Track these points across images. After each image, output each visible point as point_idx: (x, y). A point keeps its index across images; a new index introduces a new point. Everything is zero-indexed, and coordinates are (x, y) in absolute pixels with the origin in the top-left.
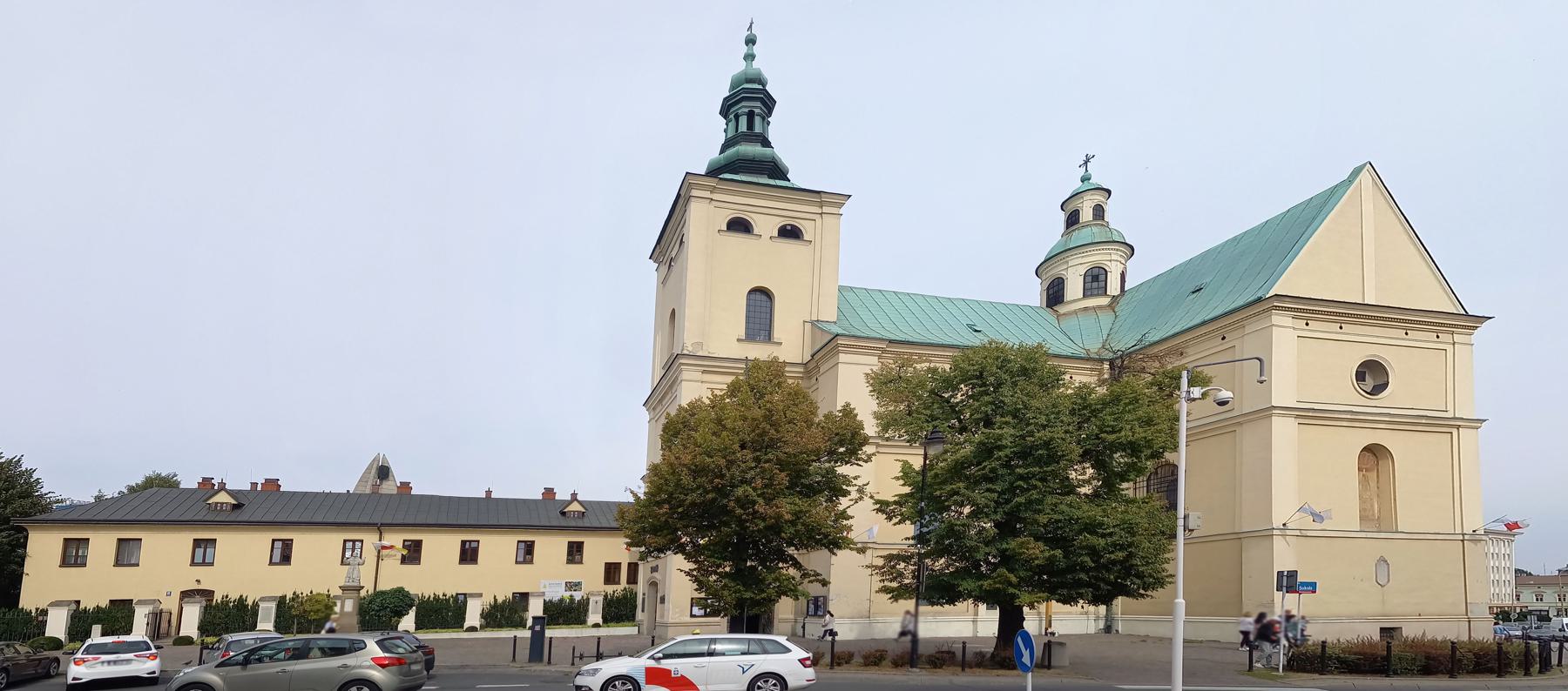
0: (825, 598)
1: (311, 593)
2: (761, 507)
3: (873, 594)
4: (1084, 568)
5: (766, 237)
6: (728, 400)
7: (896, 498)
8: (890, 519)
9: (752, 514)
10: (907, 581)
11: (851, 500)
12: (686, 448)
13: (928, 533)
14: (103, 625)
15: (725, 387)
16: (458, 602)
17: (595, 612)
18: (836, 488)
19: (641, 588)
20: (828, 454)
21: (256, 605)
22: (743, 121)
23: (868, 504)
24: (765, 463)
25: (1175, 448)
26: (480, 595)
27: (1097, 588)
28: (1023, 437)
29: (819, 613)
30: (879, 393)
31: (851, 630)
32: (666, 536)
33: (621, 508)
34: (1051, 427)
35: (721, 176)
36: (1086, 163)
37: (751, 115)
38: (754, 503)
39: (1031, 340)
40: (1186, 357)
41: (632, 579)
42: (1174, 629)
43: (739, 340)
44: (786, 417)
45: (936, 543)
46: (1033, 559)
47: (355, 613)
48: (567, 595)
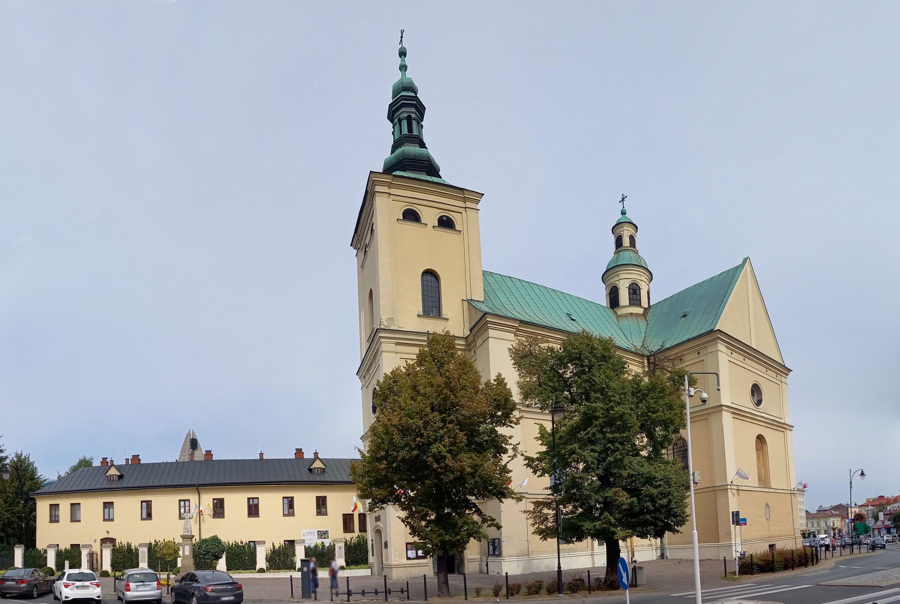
0: (499, 540)
1: (164, 541)
2: (450, 462)
3: (530, 535)
4: (649, 512)
5: (430, 226)
6: (418, 369)
7: (538, 455)
8: (535, 472)
9: (444, 468)
10: (550, 525)
11: (509, 457)
12: (394, 411)
13: (560, 484)
14: (69, 561)
15: (415, 357)
16: (250, 548)
17: (340, 557)
18: (497, 446)
19: (370, 535)
20: (491, 417)
21: (137, 550)
22: (405, 124)
23: (520, 461)
24: (449, 424)
25: (685, 426)
26: (264, 542)
27: (656, 525)
28: (608, 410)
29: (497, 553)
30: (519, 366)
31: (518, 566)
32: (386, 488)
33: (352, 464)
34: (623, 404)
35: (394, 173)
36: (623, 200)
37: (409, 119)
38: (445, 458)
39: (606, 335)
40: (683, 362)
41: (363, 529)
42: (694, 554)
43: (419, 316)
44: (460, 384)
45: (566, 492)
46: (622, 505)
47: (191, 556)
48: (319, 541)
